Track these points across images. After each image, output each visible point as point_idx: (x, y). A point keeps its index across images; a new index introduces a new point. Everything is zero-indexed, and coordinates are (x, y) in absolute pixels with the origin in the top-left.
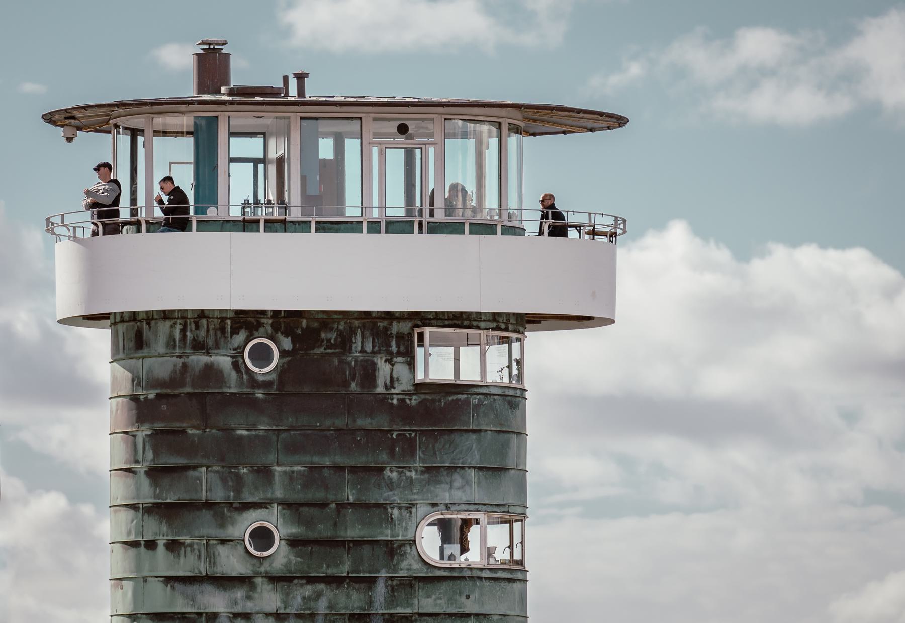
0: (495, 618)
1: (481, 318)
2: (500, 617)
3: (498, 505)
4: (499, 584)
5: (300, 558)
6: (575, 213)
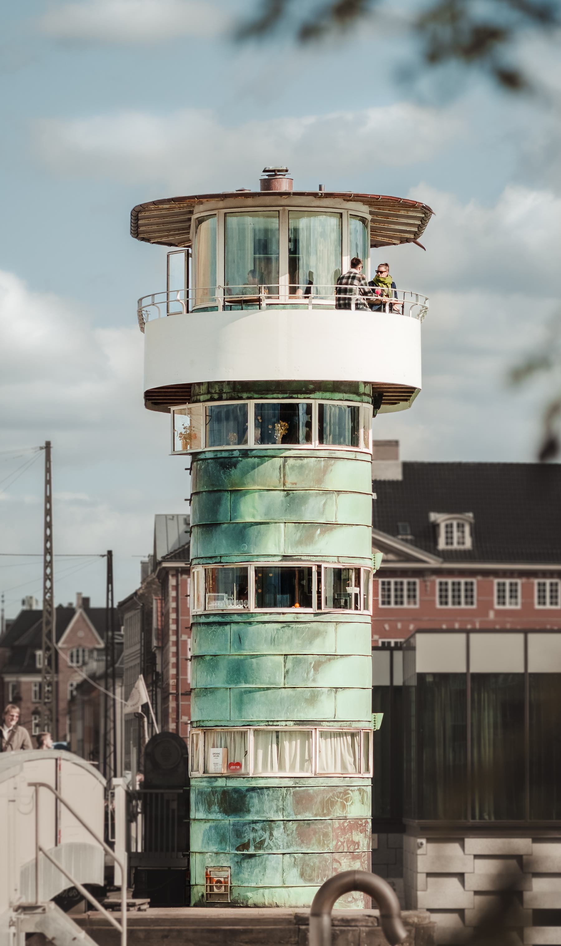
0: (208, 658)
1: (200, 392)
2: (211, 657)
3: (211, 558)
4: (211, 627)
5: (130, 741)
6: (44, 451)
